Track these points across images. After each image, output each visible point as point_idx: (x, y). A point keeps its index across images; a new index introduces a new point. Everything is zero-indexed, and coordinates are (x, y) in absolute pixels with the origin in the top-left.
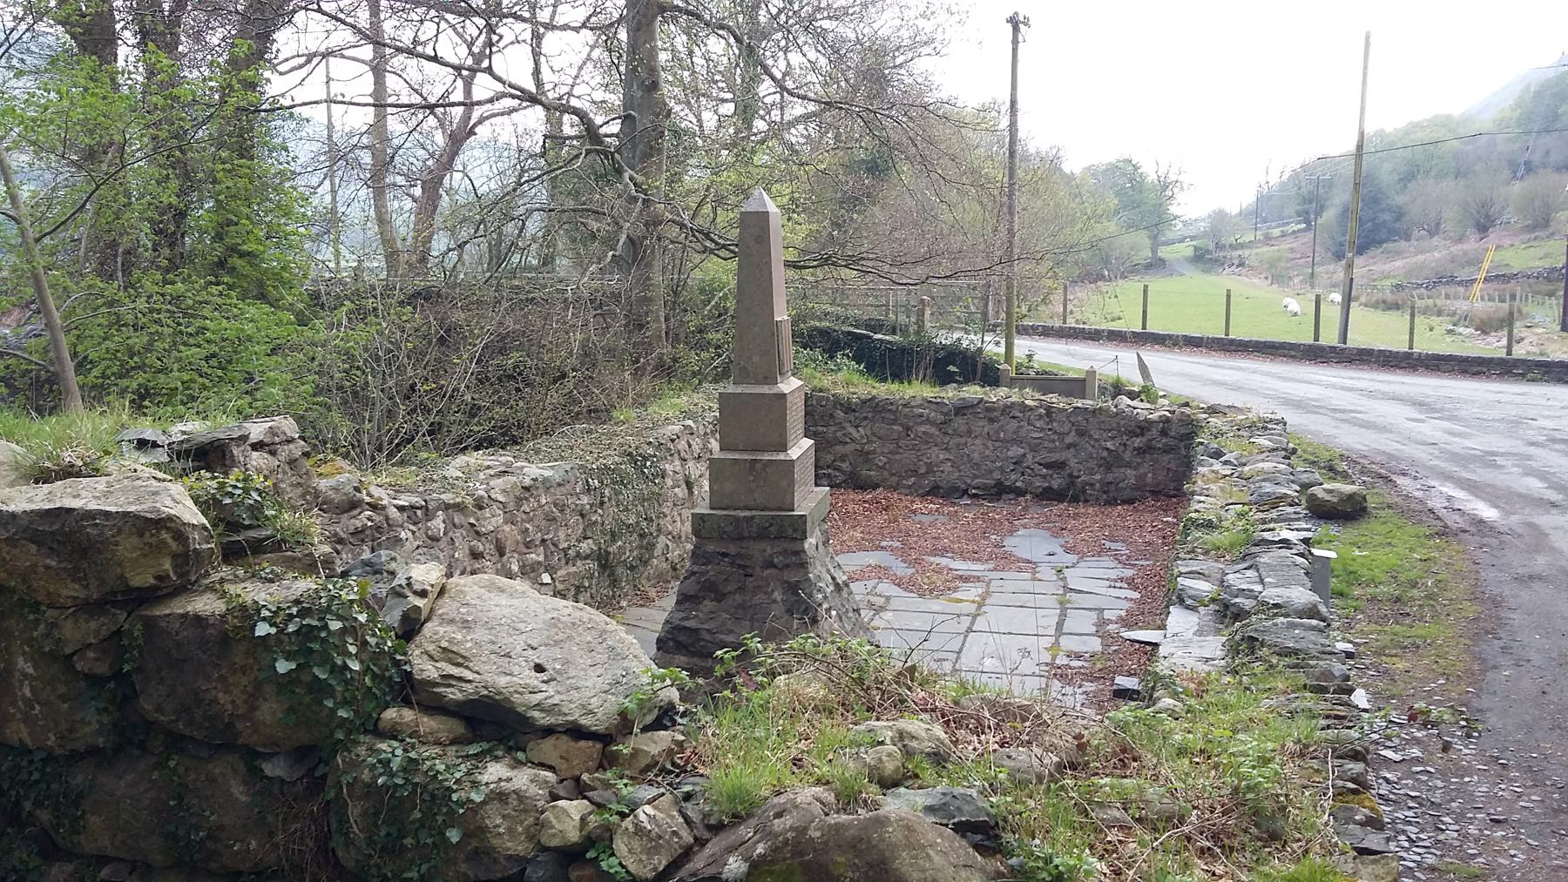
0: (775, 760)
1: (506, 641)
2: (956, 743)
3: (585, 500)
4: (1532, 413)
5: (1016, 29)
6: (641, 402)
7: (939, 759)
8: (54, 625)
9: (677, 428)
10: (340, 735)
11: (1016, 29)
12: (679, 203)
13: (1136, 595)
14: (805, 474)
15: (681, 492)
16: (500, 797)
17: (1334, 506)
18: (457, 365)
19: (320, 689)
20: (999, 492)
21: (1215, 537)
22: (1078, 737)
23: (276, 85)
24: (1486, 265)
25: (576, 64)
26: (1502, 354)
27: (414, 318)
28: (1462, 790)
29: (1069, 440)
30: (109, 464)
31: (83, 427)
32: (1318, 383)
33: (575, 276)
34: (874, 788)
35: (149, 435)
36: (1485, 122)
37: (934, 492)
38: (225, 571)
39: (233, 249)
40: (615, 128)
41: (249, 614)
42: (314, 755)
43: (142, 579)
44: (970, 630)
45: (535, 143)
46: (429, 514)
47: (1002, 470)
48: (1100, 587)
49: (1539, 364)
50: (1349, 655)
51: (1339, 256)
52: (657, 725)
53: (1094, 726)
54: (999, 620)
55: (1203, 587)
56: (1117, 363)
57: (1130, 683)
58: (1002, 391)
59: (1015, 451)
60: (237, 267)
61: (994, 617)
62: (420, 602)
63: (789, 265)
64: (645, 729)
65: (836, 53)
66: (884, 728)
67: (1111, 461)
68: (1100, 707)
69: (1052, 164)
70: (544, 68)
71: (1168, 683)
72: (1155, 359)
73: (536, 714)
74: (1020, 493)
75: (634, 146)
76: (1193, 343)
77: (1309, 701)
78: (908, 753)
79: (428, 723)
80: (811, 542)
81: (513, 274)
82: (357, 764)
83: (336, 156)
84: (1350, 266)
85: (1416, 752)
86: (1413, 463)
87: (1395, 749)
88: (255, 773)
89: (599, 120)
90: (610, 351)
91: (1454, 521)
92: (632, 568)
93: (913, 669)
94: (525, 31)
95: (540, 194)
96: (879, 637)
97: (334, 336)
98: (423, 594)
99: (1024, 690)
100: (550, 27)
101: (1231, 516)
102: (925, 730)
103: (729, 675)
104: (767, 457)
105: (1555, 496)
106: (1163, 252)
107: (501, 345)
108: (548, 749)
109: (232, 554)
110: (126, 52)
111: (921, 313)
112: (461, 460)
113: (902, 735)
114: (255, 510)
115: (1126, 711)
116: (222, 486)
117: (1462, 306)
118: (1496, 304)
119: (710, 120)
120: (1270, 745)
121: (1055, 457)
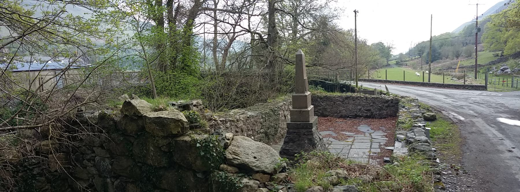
0: (309, 180)
1: (247, 151)
2: (349, 175)
3: (262, 120)
4: (470, 96)
5: (356, 14)
6: (274, 98)
7: (346, 178)
8: (158, 141)
9: (282, 104)
10: (212, 169)
11: (356, 14)
12: (281, 53)
13: (387, 139)
14: (312, 114)
15: (283, 118)
16: (247, 186)
17: (429, 118)
18: (233, 88)
19: (208, 159)
20: (356, 116)
21: (404, 125)
22: (377, 172)
23: (194, 31)
24: (458, 65)
25: (257, 23)
26: (463, 84)
27: (222, 79)
28: (460, 180)
29: (371, 104)
30: (168, 108)
31: (162, 101)
32: (424, 91)
33: (257, 70)
34: (331, 186)
35: (174, 103)
36: (457, 33)
37: (341, 117)
38: (190, 132)
39: (186, 65)
40: (266, 37)
41: (195, 141)
42: (207, 173)
43: (175, 132)
44: (351, 148)
45: (249, 41)
46: (226, 122)
47: (356, 112)
48: (379, 137)
49: (471, 86)
50: (435, 151)
51: (427, 63)
52: (282, 172)
53: (380, 169)
54: (358, 146)
55: (402, 137)
56: (381, 87)
57: (388, 159)
58: (356, 94)
59: (359, 107)
60: (186, 68)
61: (356, 145)
62: (228, 141)
63: (307, 66)
64: (280, 172)
65: (315, 18)
66: (333, 172)
67: (381, 109)
68: (380, 164)
69: (364, 43)
70: (251, 25)
71: (396, 159)
72: (389, 86)
73: (254, 168)
74: (361, 117)
75: (270, 41)
76: (397, 82)
77: (427, 162)
78: (339, 177)
79: (230, 168)
80: (314, 129)
81: (244, 70)
82: (215, 176)
83: (206, 45)
84: (430, 65)
85: (450, 172)
86: (446, 108)
87: (445, 171)
88: (195, 176)
89: (263, 35)
90: (266, 87)
91: (455, 120)
92: (273, 136)
93: (339, 158)
94: (247, 16)
95: (250, 52)
96: (331, 151)
97: (208, 83)
98: (229, 139)
99: (364, 161)
100: (252, 15)
101: (408, 121)
102: (342, 172)
103: (298, 160)
104: (303, 110)
105: (476, 115)
106: (389, 62)
107: (241, 85)
108: (257, 176)
109: (192, 128)
110: (166, 25)
111: (337, 76)
112: (233, 111)
113: (337, 173)
114: (196, 119)
115: (387, 166)
116: (190, 113)
117: (454, 74)
118: (461, 73)
119: (287, 34)
120: (419, 172)
121: (368, 108)
